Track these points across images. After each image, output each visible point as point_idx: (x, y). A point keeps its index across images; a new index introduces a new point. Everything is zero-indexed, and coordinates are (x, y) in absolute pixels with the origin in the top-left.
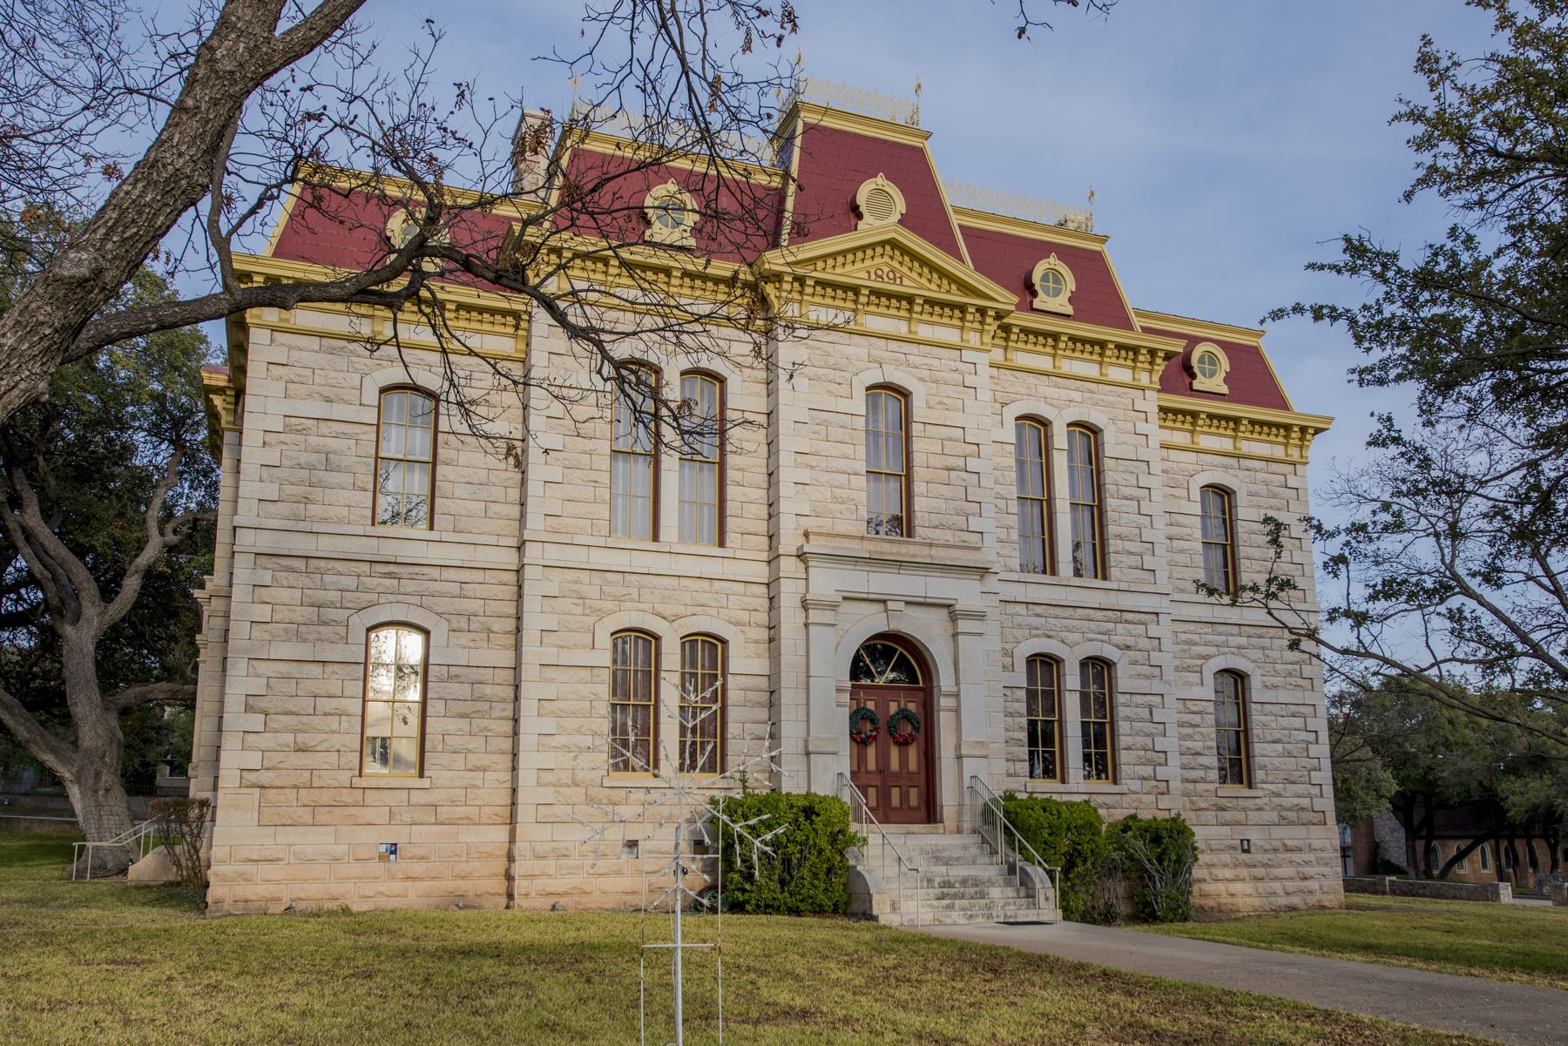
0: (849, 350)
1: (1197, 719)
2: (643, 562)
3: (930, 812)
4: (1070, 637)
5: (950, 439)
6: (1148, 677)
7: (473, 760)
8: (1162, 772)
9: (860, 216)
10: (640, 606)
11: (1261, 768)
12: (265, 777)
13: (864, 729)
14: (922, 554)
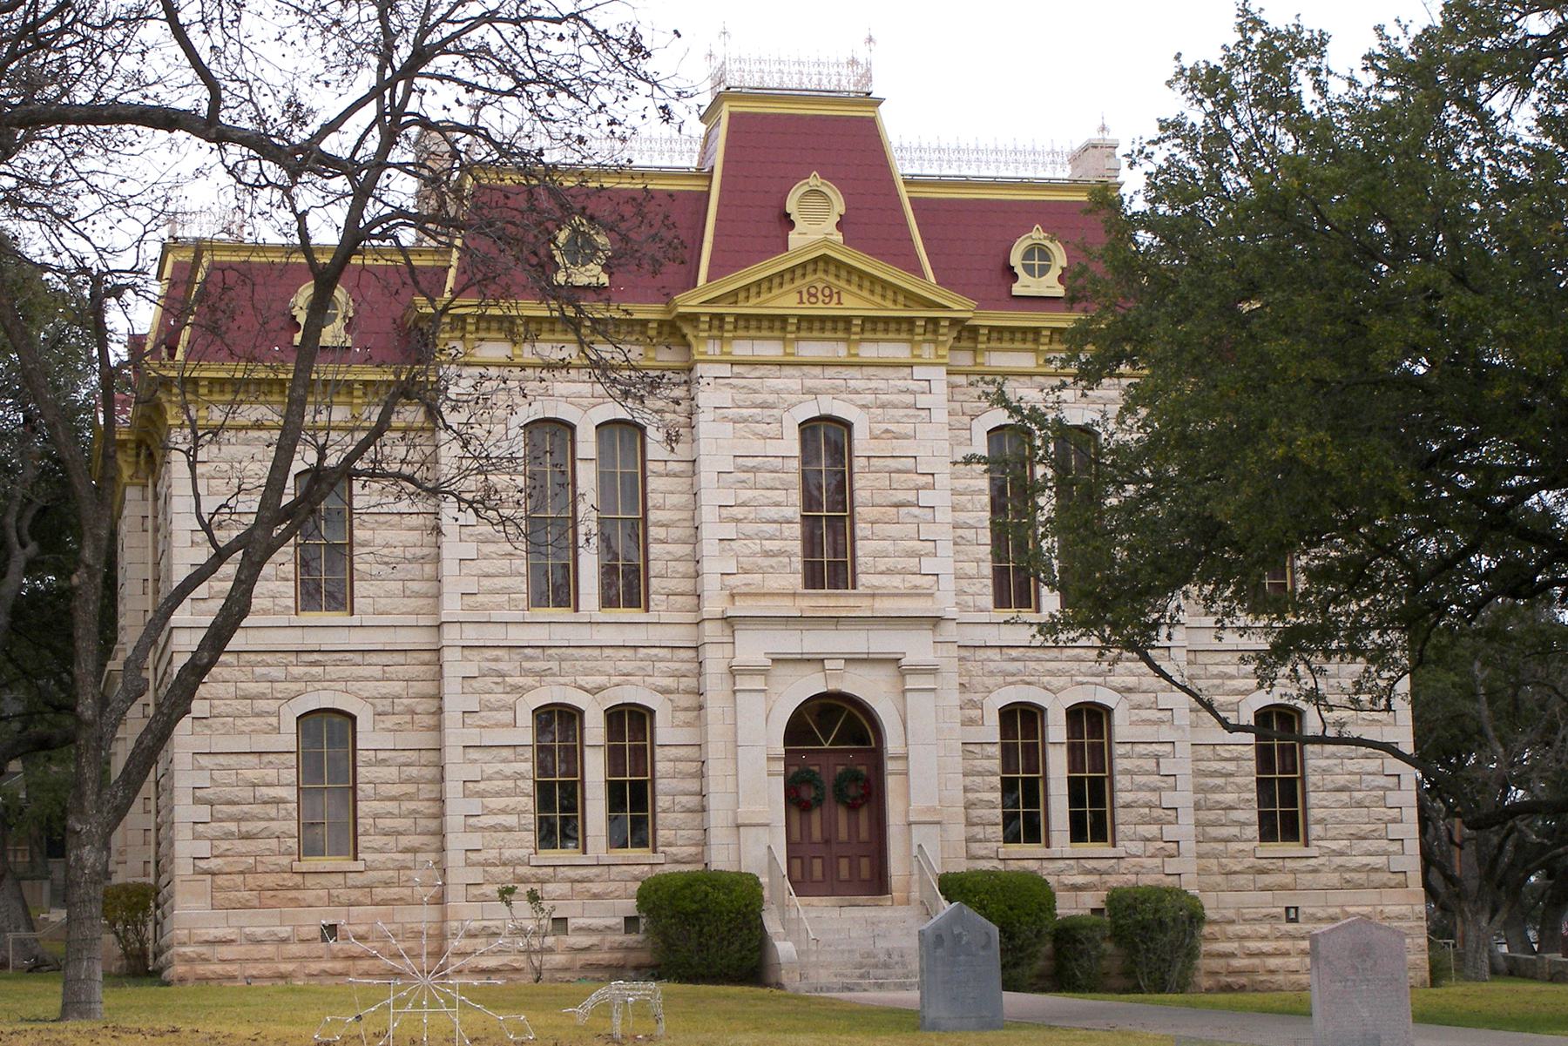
0: (778, 384)
1: (1230, 767)
2: (560, 635)
3: (878, 884)
4: (1056, 682)
5: (899, 471)
6: (1155, 723)
7: (405, 841)
8: (1170, 832)
9: (792, 225)
10: (562, 680)
11: (1319, 822)
12: (213, 864)
13: (800, 794)
14: (865, 607)
